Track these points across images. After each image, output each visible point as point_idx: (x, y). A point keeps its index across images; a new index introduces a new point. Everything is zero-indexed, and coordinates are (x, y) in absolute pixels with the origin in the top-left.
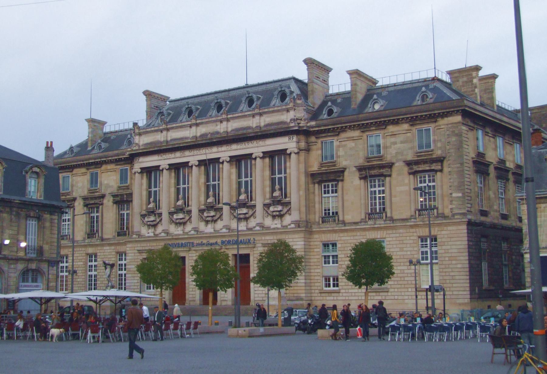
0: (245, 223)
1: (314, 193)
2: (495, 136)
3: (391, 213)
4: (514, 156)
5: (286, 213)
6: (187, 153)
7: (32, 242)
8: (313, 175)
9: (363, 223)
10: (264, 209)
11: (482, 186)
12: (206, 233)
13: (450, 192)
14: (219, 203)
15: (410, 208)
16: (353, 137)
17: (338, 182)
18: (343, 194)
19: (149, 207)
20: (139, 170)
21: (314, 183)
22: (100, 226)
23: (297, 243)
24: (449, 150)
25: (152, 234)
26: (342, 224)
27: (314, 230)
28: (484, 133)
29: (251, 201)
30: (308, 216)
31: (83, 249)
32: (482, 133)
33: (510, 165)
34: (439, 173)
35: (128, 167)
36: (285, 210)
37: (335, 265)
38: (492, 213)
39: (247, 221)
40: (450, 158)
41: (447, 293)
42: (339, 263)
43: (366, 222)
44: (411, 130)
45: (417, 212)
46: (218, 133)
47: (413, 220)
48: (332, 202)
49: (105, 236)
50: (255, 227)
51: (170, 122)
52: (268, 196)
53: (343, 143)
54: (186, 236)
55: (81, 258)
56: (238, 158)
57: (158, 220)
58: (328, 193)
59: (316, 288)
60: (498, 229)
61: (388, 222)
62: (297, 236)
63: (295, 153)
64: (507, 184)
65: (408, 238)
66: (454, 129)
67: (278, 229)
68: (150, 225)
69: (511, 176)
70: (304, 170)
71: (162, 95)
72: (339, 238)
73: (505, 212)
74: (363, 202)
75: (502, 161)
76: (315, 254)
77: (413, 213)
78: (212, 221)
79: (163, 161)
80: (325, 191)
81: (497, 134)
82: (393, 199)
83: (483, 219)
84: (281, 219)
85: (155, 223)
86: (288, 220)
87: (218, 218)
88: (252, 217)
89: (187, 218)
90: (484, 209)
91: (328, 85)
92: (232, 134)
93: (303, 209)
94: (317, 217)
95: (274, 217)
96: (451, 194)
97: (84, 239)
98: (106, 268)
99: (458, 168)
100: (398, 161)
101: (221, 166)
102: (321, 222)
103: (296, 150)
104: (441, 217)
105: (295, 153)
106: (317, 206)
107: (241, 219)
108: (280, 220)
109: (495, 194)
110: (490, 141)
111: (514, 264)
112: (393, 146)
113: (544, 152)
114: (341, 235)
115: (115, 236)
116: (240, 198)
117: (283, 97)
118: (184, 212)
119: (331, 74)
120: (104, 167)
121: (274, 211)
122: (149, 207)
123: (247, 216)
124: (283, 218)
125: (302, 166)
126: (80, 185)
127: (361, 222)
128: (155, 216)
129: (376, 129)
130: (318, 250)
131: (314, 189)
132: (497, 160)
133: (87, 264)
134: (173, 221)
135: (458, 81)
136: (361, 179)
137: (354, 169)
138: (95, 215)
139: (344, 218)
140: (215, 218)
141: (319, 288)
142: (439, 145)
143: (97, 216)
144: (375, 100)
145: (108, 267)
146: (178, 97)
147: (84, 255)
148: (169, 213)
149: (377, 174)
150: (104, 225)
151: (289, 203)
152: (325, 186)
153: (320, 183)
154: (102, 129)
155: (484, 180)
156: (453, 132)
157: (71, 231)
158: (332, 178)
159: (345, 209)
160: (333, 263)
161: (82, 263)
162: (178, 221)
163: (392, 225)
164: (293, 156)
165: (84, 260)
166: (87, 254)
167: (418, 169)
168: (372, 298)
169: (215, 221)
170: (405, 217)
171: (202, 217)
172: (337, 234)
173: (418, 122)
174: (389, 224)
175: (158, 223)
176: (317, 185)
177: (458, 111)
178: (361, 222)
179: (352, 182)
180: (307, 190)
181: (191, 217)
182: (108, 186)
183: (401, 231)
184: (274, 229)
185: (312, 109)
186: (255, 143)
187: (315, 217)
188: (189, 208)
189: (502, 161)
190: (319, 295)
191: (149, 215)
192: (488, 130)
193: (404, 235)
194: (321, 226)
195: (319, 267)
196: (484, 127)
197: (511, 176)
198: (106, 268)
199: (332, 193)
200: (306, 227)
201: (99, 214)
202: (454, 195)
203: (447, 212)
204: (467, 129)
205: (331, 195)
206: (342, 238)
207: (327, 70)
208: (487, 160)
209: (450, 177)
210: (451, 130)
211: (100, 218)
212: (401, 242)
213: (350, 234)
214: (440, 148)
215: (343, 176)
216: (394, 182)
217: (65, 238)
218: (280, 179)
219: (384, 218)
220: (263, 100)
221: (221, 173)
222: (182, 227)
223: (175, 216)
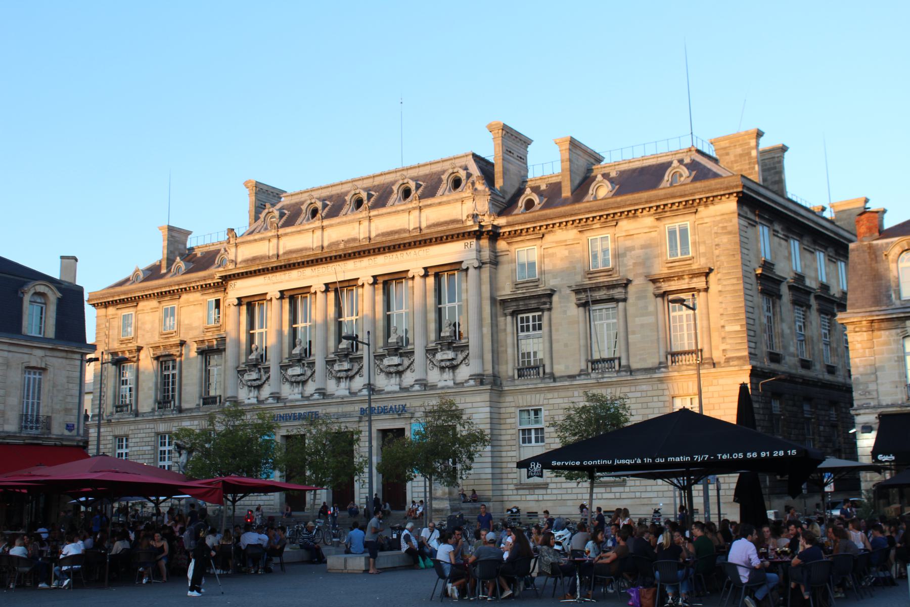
0: (398, 379)
2: (788, 237)
3: (628, 359)
4: (816, 270)
6: (308, 271)
7: (33, 410)
9: (583, 377)
11: (771, 314)
12: (338, 397)
13: (722, 323)
15: (659, 352)
16: (566, 241)
18: (550, 331)
19: (250, 357)
21: (505, 315)
22: (177, 390)
23: (477, 410)
24: (718, 256)
25: (254, 401)
26: (550, 378)
27: (506, 388)
28: (772, 232)
29: (407, 345)
31: (152, 426)
32: (769, 230)
33: (810, 283)
34: (702, 294)
35: (219, 296)
36: (460, 357)
37: (540, 444)
38: (787, 358)
39: (400, 377)
40: (721, 270)
41: (723, 486)
42: (547, 441)
43: (588, 374)
44: (656, 227)
45: (669, 357)
47: (663, 370)
48: (534, 345)
49: (185, 406)
50: (412, 386)
53: (550, 251)
54: (306, 403)
55: (149, 439)
57: (264, 378)
58: (528, 330)
59: (510, 481)
60: (796, 383)
61: (624, 373)
62: (478, 398)
64: (808, 313)
65: (655, 399)
66: (725, 224)
67: (449, 388)
68: (251, 386)
69: (813, 302)
72: (546, 402)
73: (806, 357)
74: (582, 342)
75: (800, 278)
76: (508, 426)
77: (663, 359)
78: (346, 378)
80: (522, 327)
81: (790, 235)
82: (630, 337)
83: (774, 366)
85: (258, 383)
86: (464, 373)
89: (309, 373)
90: (777, 351)
91: (526, 164)
92: (379, 239)
93: (488, 356)
94: (508, 369)
96: (723, 327)
97: (153, 410)
98: (180, 455)
99: (733, 284)
100: (636, 276)
102: (516, 377)
104: (707, 363)
106: (510, 351)
107: (391, 373)
109: (790, 328)
110: (780, 245)
111: (823, 439)
112: (628, 253)
113: (882, 245)
114: (549, 396)
115: (198, 405)
116: (390, 341)
117: (457, 183)
118: (304, 364)
119: (530, 148)
120: (184, 297)
121: (442, 361)
122: (250, 357)
123: (400, 368)
124: (457, 371)
125: (486, 289)
126: (148, 326)
127: (579, 375)
128: (259, 369)
130: (512, 420)
131: (506, 324)
132: (792, 275)
133: (157, 448)
134: (287, 380)
135: (727, 154)
136: (579, 306)
137: (568, 291)
138: (171, 372)
139: (552, 368)
140: (350, 373)
141: (515, 481)
142: (702, 249)
143: (173, 375)
144: (599, 182)
145: (184, 452)
147: (153, 434)
149: (605, 297)
150: (183, 388)
153: (514, 314)
154: (185, 245)
155: (774, 307)
156: (724, 228)
157: (133, 398)
158: (533, 306)
159: (554, 355)
160: (537, 441)
161: (149, 448)
162: (293, 380)
163: (629, 378)
164: (471, 272)
165: (152, 443)
166: (158, 434)
167: (669, 289)
168: (599, 496)
169: (352, 378)
170: (650, 366)
172: (542, 395)
173: (668, 214)
174: (625, 377)
175: (264, 383)
176: (509, 318)
177: (730, 194)
178: (579, 375)
179: (565, 310)
180: (494, 325)
182: (190, 328)
183: (644, 387)
184: (442, 388)
185: (501, 199)
186: (412, 253)
189: (800, 278)
190: (515, 492)
191: (250, 371)
192: (777, 227)
193: (649, 394)
194: (517, 382)
195: (514, 448)
196: (771, 222)
197: (813, 302)
198: (180, 455)
199: (534, 329)
200: (492, 383)
201: (176, 372)
202: (728, 328)
203: (717, 356)
204: (746, 224)
206: (551, 401)
207: (526, 142)
208: (778, 273)
209: (721, 299)
210: (721, 225)
211: (177, 378)
212: (645, 406)
213: (563, 394)
214: (704, 254)
215: (551, 303)
216: (631, 310)
217: (125, 409)
219: (617, 368)
220: (425, 188)
222: (300, 388)
223: (290, 372)
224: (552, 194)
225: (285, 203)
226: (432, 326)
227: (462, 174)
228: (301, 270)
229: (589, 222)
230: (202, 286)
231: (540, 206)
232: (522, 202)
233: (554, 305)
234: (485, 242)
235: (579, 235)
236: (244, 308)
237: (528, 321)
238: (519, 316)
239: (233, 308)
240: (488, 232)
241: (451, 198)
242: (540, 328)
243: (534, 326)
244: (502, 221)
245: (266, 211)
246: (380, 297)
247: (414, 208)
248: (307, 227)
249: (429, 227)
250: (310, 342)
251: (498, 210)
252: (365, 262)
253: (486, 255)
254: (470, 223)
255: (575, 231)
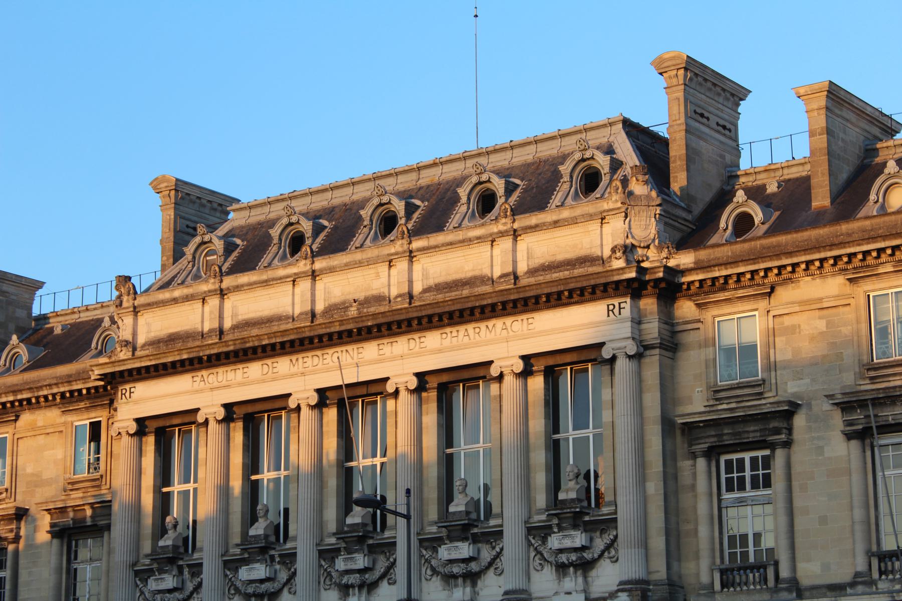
1: (693, 487)
5: (601, 556)
6: (283, 364)
8: (690, 429)
9: (860, 588)
10: (530, 544)
14: (598, 505)
16: (820, 300)
17: (773, 451)
19: (161, 543)
20: (133, 427)
21: (694, 456)
30: (675, 565)
35: (100, 415)
36: (600, 544)
39: (474, 584)
45: (875, 562)
46: (379, 299)
48: (755, 519)
51: (232, 271)
52: (541, 500)
56: (250, 409)
57: (190, 586)
58: (742, 488)
63: (630, 357)
70: (659, 413)
71: (213, 193)
74: (858, 514)
78: (361, 587)
79: (205, 393)
80: (729, 481)
84: (585, 577)
87: (382, 577)
88: (491, 573)
89: (283, 576)
91: (736, 140)
92: (430, 298)
93: (658, 543)
95: (562, 569)
101: (391, 403)
102: (717, 586)
103: (632, 349)
105: (630, 357)
106: (703, 531)
107: (454, 577)
108: (580, 580)
118: (272, 558)
119: (743, 107)
120: (26, 418)
121: (561, 551)
122: (161, 543)
123: (474, 567)
124: (593, 573)
125: (652, 401)
127: (853, 584)
128: (180, 569)
129: (87, 408)
131: (694, 475)
134: (237, 590)
136: (849, 436)
137: (827, 406)
139: (794, 568)
140: (369, 577)
144: (891, 176)
146: (261, 197)
148: (226, 564)
151: (612, 522)
152: (729, 463)
158: (752, 437)
159: (798, 541)
171: (329, 574)
176: (701, 463)
178: (853, 584)
181: (294, 574)
182: (37, 482)
185: (684, 214)
187: (698, 565)
188: (289, 545)
191: (161, 571)
199: (755, 486)
205: (749, 493)
207: (736, 95)
215: (790, 430)
218: (581, 443)
220: (525, 191)
221: (390, 430)
224: (789, 202)
225: (236, 224)
226: (540, 479)
227: (602, 162)
228: (269, 361)
229: (870, 261)
230: (63, 395)
231: (766, 226)
232: (726, 220)
233: (797, 435)
234: (649, 304)
235: (848, 288)
236: (150, 441)
237: (741, 468)
238: (723, 458)
239: (126, 439)
240: (657, 281)
241: (578, 212)
242: (767, 483)
243: (755, 479)
244: (685, 259)
245: (198, 239)
246: (431, 419)
247: (502, 234)
248: (281, 272)
249: (532, 272)
250: (286, 511)
251: (678, 236)
252: (401, 345)
253: (652, 329)
254: (619, 263)
255: (840, 280)
